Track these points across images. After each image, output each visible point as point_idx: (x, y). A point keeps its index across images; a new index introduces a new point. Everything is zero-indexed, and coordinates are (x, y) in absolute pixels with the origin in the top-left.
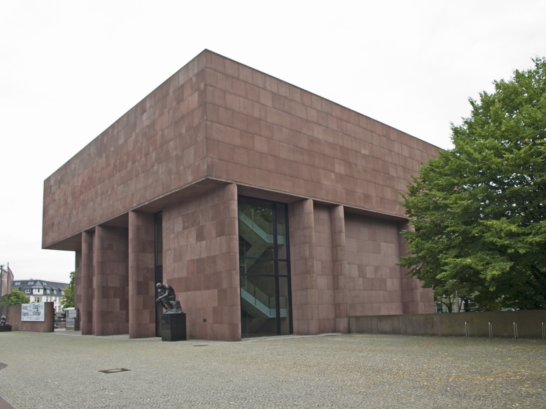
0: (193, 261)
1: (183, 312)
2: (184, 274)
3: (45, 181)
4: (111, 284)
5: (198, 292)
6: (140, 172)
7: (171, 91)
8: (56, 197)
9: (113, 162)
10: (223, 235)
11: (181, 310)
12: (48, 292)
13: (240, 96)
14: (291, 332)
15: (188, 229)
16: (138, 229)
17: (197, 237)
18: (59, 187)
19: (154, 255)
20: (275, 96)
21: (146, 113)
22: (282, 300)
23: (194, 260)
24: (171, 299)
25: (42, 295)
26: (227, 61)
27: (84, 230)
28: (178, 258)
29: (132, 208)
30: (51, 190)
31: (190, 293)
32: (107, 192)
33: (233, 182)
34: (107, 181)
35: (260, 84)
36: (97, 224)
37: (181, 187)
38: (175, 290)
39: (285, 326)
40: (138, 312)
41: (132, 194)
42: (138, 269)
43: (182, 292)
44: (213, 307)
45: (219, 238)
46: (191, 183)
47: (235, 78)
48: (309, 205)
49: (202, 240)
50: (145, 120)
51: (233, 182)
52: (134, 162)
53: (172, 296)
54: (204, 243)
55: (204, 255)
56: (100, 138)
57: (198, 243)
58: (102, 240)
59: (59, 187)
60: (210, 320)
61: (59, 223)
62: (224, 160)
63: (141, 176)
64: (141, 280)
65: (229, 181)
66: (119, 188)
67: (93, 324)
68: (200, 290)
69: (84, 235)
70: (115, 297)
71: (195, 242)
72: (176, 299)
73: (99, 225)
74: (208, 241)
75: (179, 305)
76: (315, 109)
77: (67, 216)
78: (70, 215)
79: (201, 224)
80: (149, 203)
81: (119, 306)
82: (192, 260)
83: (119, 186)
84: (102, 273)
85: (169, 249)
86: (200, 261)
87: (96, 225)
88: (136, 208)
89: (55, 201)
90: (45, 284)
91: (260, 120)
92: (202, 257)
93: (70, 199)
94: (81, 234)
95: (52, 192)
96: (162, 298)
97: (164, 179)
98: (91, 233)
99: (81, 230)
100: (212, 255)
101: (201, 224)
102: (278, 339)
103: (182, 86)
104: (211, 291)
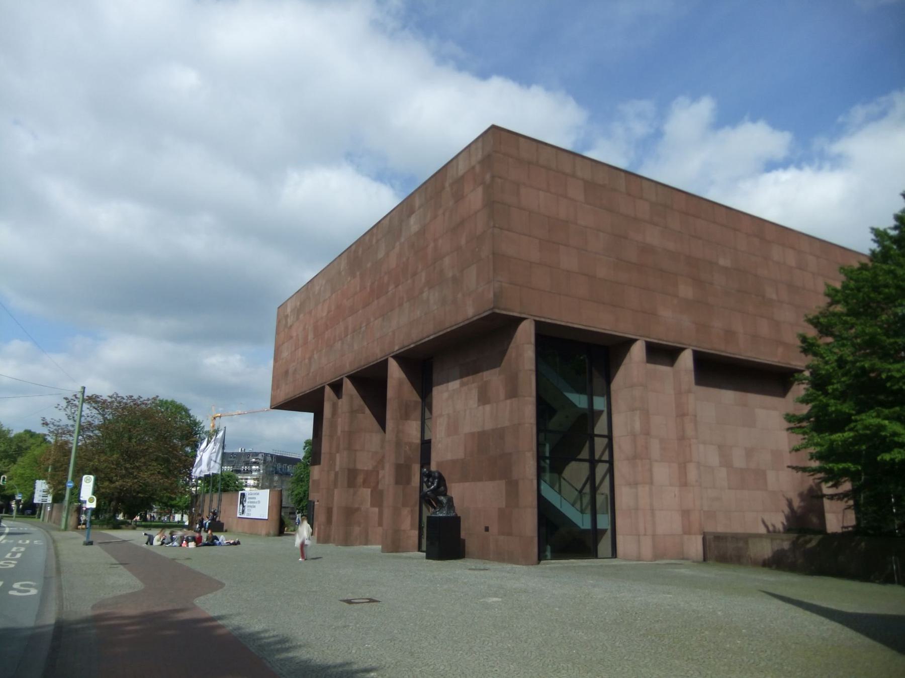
0: (473, 434)
7: (447, 185)
9: (369, 284)
11: (454, 511)
20: (590, 186)
21: (414, 215)
32: (361, 328)
33: (529, 317)
34: (360, 311)
39: (604, 545)
45: (508, 401)
51: (529, 317)
54: (488, 407)
55: (489, 426)
57: (481, 408)
61: (295, 370)
64: (402, 462)
72: (448, 494)
77: (307, 361)
83: (376, 319)
87: (344, 376)
89: (291, 337)
98: (337, 387)
100: (499, 426)
101: (485, 379)
103: (463, 177)
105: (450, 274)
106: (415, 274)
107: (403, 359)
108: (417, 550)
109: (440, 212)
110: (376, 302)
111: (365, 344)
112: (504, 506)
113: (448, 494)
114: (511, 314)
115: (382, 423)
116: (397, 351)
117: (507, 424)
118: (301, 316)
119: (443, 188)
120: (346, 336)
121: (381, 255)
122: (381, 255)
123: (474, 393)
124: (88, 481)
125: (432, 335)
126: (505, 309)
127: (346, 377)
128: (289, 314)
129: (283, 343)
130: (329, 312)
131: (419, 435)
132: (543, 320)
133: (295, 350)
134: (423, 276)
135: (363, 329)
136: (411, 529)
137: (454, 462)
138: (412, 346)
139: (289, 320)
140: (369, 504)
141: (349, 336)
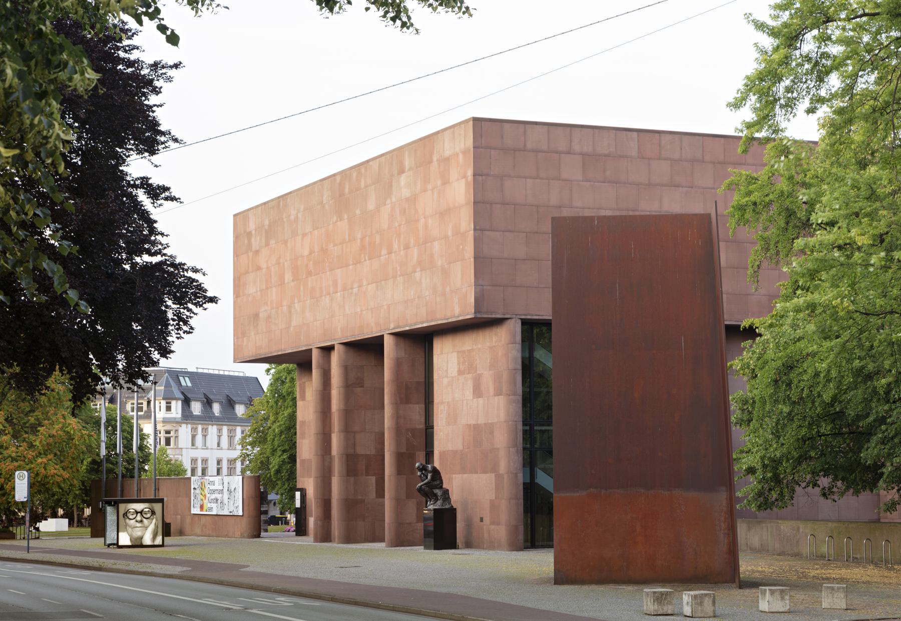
4: (361, 450)
5: (475, 476)
6: (399, 273)
8: (262, 262)
9: (359, 236)
10: (501, 395)
11: (450, 503)
12: (196, 408)
13: (526, 178)
17: (473, 391)
18: (267, 244)
19: (423, 406)
20: (589, 159)
23: (470, 425)
24: (436, 487)
25: (179, 423)
26: (506, 125)
28: (453, 419)
30: (250, 243)
31: (466, 475)
32: (352, 289)
33: (514, 316)
34: (351, 267)
35: (562, 146)
37: (447, 319)
38: (441, 472)
40: (399, 503)
41: (389, 306)
42: (398, 431)
43: (457, 474)
44: (490, 500)
45: (496, 398)
46: (458, 317)
47: (520, 150)
49: (480, 397)
51: (514, 316)
52: (390, 253)
53: (438, 482)
54: (481, 400)
55: (481, 421)
57: (475, 400)
58: (346, 369)
59: (267, 244)
60: (487, 520)
61: (269, 317)
62: (499, 286)
63: (400, 279)
64: (404, 450)
65: (506, 316)
66: (370, 287)
67: (333, 522)
68: (477, 473)
70: (367, 474)
71: (472, 398)
72: (444, 487)
74: (486, 399)
75: (447, 496)
76: (665, 159)
77: (285, 308)
78: (290, 307)
79: (478, 372)
81: (375, 490)
82: (468, 425)
83: (369, 284)
84: (347, 430)
85: (442, 403)
89: (259, 268)
90: (186, 382)
91: (560, 207)
92: (479, 423)
93: (288, 277)
96: (422, 485)
97: (428, 298)
98: (327, 350)
100: (490, 422)
101: (478, 372)
104: (488, 475)
107: (401, 336)
109: (429, 187)
111: (359, 310)
112: (494, 498)
113: (444, 486)
114: (494, 316)
117: (495, 420)
121: (371, 206)
124: (22, 477)
126: (487, 312)
128: (253, 232)
129: (247, 272)
131: (423, 419)
132: (529, 317)
133: (267, 288)
135: (355, 290)
136: (417, 522)
137: (455, 452)
138: (407, 328)
139: (253, 240)
140: (374, 495)
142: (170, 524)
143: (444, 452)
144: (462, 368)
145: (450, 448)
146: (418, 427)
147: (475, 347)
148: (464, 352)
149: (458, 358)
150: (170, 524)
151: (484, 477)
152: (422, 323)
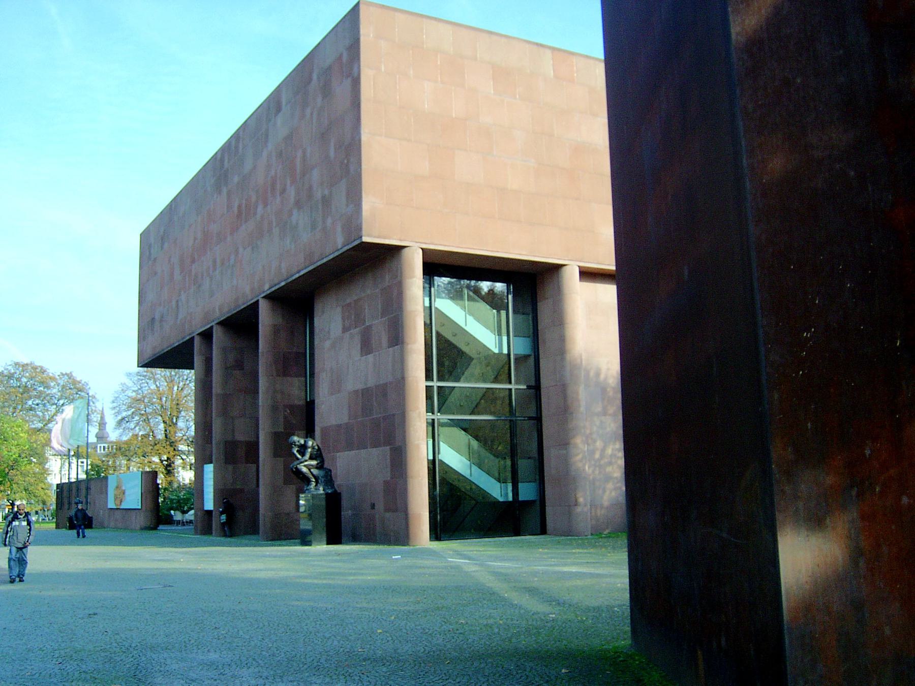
0: (356, 392)
1: (336, 491)
2: (345, 419)
3: (145, 236)
7: (315, 77)
9: (236, 205)
14: (543, 531)
15: (348, 332)
16: (276, 330)
17: (361, 348)
21: (280, 114)
22: (524, 465)
27: (197, 333)
28: (336, 386)
29: (264, 292)
36: (216, 322)
39: (532, 518)
48: (571, 275)
50: (280, 127)
54: (370, 357)
55: (371, 383)
56: (219, 156)
60: (380, 506)
64: (281, 429)
68: (365, 447)
69: (197, 342)
73: (219, 324)
80: (287, 284)
83: (245, 249)
86: (366, 393)
87: (213, 324)
88: (268, 292)
89: (156, 273)
92: (369, 385)
93: (177, 271)
94: (192, 339)
95: (153, 257)
98: (207, 335)
99: (193, 333)
102: (165, 529)
103: (330, 68)
105: (318, 194)
106: (284, 191)
107: (277, 298)
108: (325, 542)
110: (244, 226)
115: (565, 265)
116: (268, 290)
118: (166, 245)
119: (310, 80)
120: (215, 269)
122: (248, 165)
123: (357, 340)
125: (303, 270)
127: (217, 324)
130: (195, 239)
134: (291, 192)
137: (339, 426)
138: (283, 284)
141: (217, 272)
142: (92, 517)
143: (326, 427)
144: (347, 323)
145: (334, 423)
146: (297, 402)
147: (363, 295)
148: (349, 305)
149: (343, 312)
150: (92, 517)
151: (375, 452)
152: (298, 272)
